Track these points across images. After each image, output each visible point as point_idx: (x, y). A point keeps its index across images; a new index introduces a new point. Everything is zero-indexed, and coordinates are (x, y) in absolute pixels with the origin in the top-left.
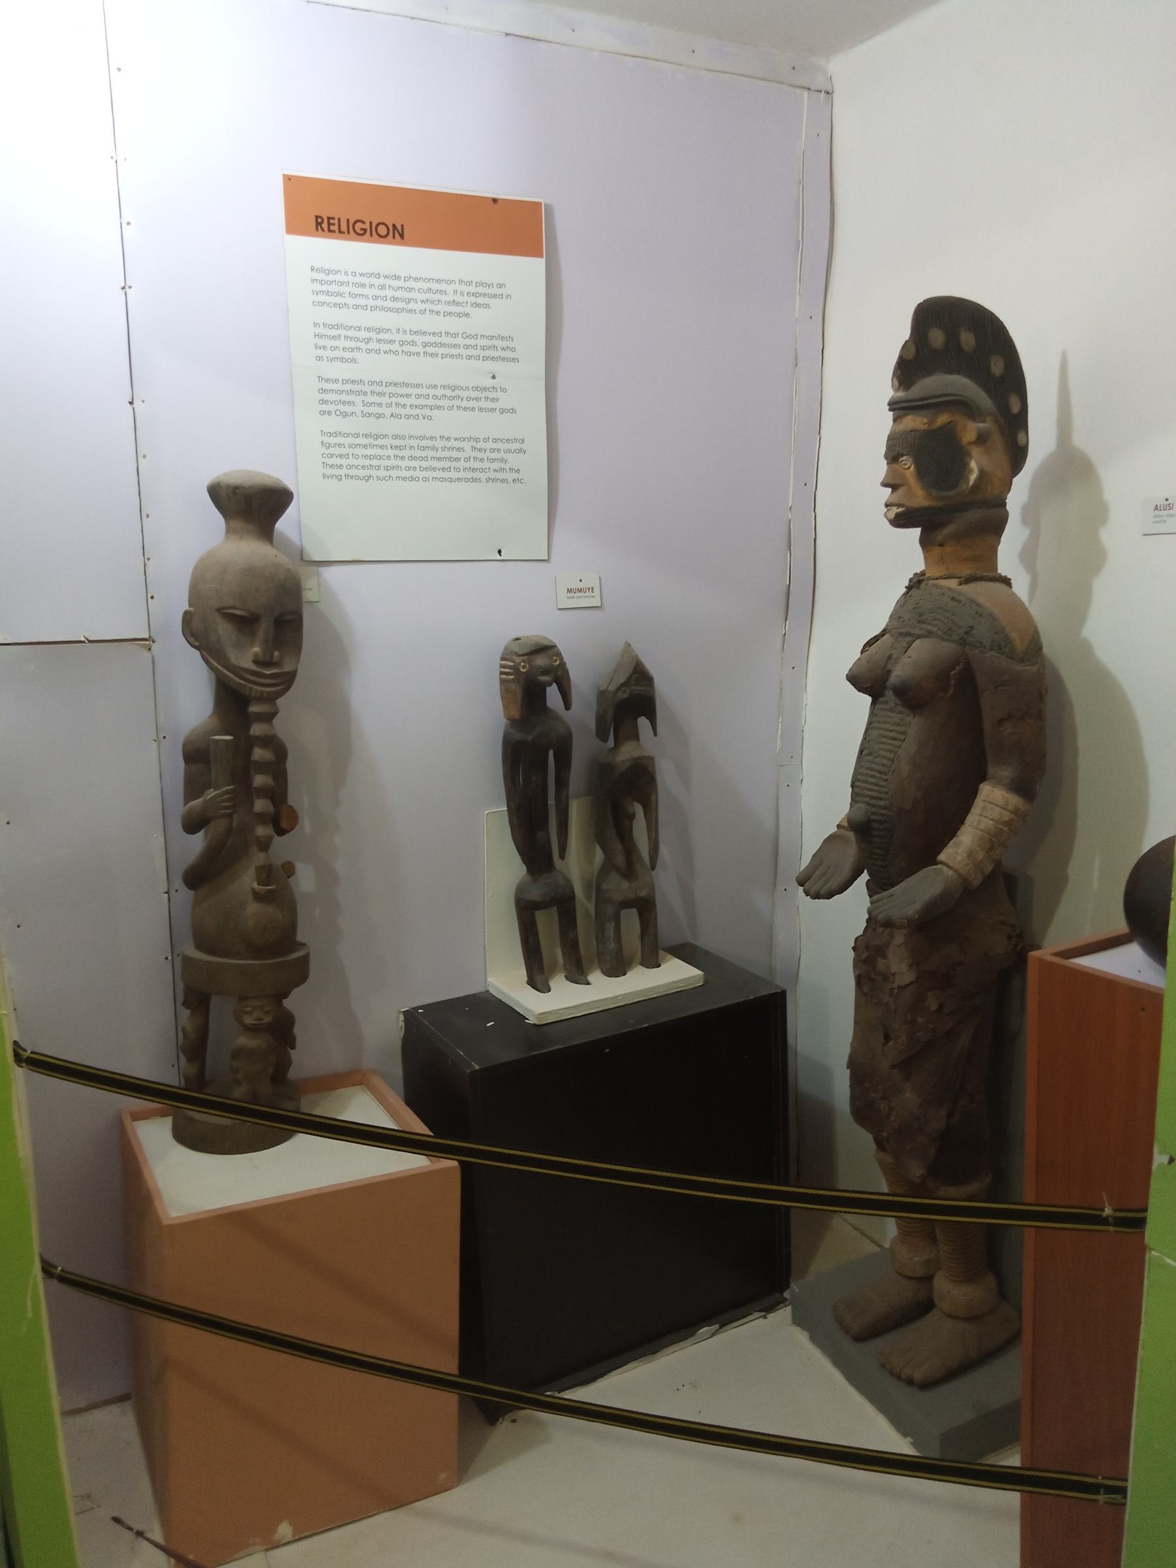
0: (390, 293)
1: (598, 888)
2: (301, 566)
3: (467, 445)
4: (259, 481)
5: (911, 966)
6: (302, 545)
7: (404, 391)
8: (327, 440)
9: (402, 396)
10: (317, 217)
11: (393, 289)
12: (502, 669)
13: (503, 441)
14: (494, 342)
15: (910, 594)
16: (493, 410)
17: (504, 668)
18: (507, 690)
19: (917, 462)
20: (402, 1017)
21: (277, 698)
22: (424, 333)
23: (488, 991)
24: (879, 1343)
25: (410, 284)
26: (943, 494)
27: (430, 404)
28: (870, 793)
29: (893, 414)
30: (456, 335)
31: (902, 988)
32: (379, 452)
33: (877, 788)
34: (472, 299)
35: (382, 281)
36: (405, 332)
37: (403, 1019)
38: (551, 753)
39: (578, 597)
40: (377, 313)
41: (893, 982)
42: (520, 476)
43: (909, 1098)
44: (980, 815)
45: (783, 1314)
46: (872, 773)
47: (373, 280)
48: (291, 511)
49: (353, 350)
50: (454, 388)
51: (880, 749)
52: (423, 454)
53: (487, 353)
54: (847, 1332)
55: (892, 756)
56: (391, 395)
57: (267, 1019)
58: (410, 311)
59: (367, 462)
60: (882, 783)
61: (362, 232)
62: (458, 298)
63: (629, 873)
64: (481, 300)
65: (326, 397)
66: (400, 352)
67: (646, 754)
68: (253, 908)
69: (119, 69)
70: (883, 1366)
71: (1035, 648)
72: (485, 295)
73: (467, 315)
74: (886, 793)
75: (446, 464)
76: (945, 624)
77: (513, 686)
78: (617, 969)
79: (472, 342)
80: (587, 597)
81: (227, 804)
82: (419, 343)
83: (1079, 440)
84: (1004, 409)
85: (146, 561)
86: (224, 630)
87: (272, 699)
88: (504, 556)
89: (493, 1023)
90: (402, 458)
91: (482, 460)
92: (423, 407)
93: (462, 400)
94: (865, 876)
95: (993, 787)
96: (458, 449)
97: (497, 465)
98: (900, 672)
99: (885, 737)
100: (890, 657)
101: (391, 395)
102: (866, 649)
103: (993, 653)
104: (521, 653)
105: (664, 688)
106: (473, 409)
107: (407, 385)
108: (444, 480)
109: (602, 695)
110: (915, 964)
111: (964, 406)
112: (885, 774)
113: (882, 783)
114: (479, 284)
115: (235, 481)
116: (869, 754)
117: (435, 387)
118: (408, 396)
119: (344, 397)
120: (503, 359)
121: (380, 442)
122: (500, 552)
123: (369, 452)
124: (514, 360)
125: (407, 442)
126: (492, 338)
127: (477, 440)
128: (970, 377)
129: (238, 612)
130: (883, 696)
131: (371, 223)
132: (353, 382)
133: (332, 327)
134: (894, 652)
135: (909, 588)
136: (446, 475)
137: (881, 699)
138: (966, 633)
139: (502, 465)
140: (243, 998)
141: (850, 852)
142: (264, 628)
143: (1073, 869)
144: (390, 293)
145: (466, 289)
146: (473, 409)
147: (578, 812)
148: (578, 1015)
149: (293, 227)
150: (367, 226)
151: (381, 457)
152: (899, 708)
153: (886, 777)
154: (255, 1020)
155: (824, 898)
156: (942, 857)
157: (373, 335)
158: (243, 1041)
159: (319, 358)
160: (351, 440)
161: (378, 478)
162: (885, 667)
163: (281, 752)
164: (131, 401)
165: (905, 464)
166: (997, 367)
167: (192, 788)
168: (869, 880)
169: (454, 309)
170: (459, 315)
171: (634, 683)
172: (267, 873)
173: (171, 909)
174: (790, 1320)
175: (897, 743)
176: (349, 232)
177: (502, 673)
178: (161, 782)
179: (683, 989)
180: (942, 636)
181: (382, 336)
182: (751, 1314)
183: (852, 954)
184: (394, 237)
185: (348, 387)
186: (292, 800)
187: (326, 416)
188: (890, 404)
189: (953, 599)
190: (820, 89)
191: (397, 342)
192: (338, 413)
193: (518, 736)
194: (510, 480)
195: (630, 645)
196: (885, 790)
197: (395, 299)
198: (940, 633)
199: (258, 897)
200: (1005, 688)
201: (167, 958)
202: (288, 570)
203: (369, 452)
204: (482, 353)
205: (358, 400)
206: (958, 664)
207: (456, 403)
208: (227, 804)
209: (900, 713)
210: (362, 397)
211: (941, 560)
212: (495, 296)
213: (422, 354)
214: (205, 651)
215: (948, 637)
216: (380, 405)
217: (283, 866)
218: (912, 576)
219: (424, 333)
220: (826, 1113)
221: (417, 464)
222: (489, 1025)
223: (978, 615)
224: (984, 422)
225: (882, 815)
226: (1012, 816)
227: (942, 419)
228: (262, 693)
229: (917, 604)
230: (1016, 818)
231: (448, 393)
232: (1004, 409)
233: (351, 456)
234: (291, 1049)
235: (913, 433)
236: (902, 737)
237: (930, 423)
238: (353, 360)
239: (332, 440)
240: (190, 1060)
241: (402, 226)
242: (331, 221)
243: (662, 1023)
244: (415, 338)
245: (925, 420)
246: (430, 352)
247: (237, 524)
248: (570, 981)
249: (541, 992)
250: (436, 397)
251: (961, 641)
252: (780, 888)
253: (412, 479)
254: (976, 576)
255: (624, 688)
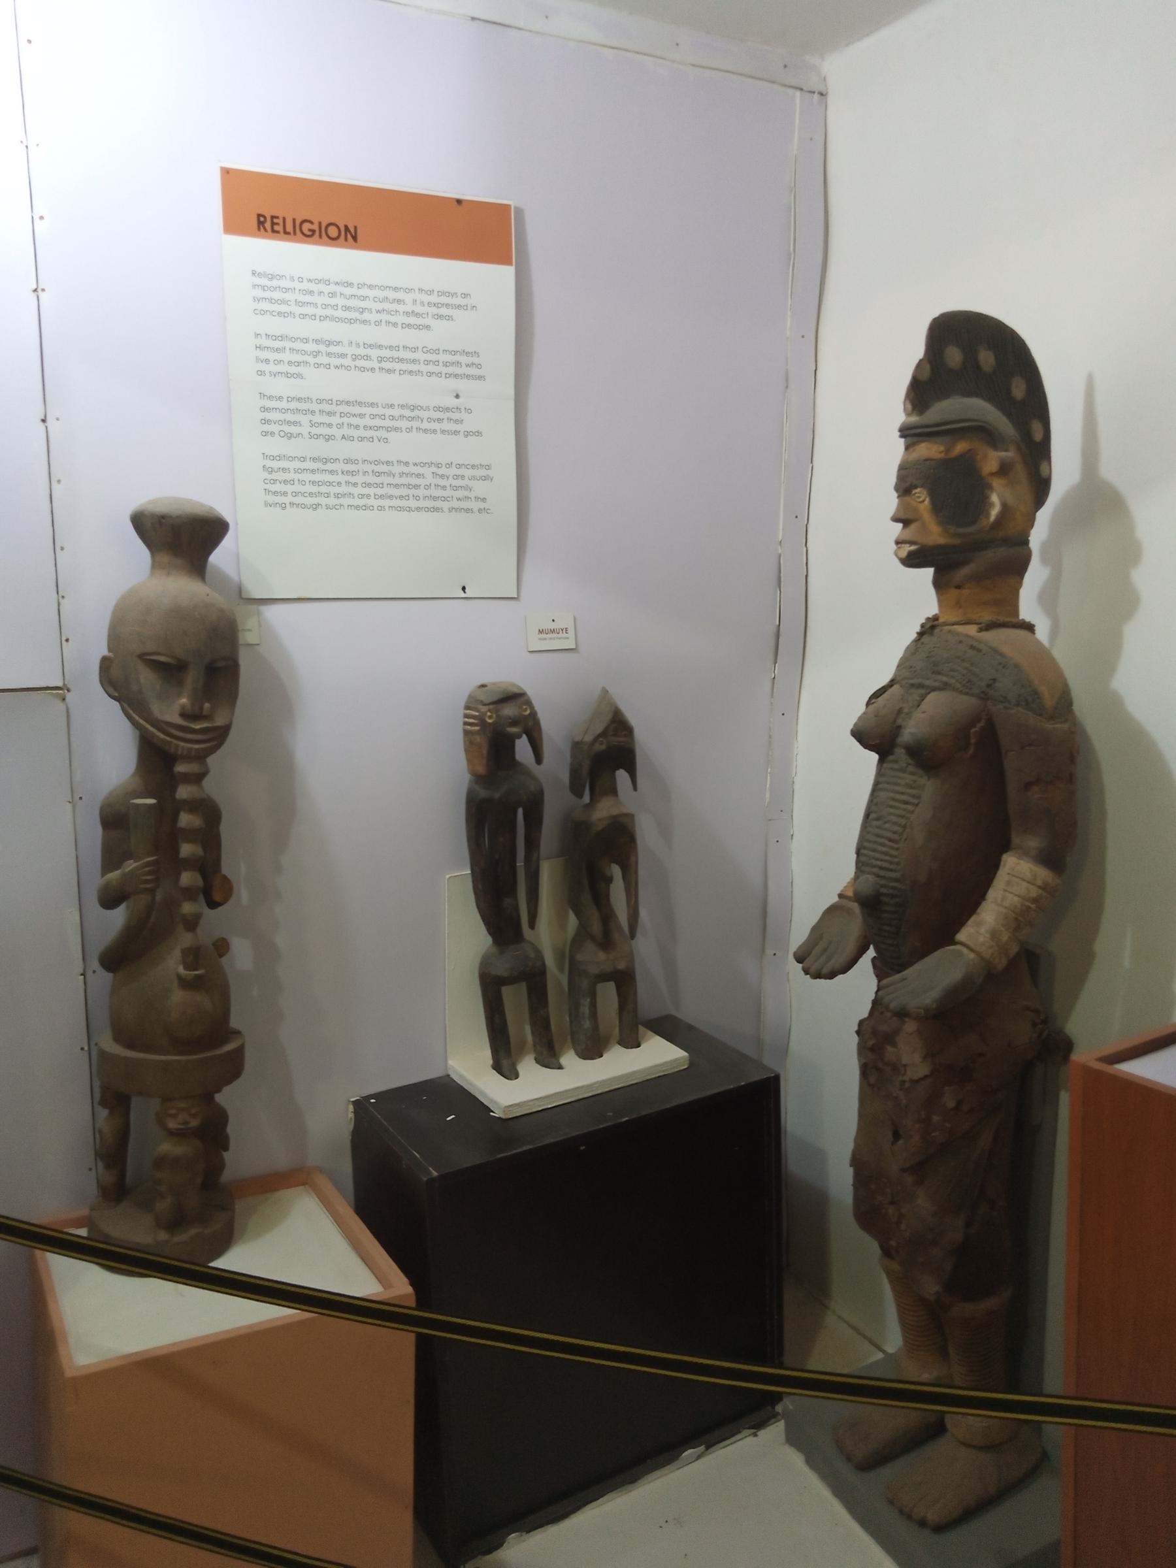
0: (341, 302)
1: (573, 962)
2: (238, 604)
3: (427, 471)
4: (189, 509)
5: (925, 1058)
6: (240, 581)
7: (356, 410)
8: (269, 463)
9: (354, 415)
10: (259, 216)
11: (345, 297)
12: (466, 720)
13: (468, 467)
14: (457, 358)
15: (922, 640)
16: (456, 433)
17: (468, 718)
18: (471, 743)
19: (932, 495)
20: (351, 1108)
21: (207, 756)
22: (380, 347)
23: (449, 1075)
24: (888, 1472)
25: (364, 292)
26: (961, 530)
27: (386, 425)
28: (879, 863)
29: (905, 441)
30: (415, 349)
31: (916, 1082)
32: (328, 478)
33: (887, 858)
34: (434, 310)
35: (332, 288)
36: (358, 345)
37: (353, 1110)
38: (520, 811)
39: (551, 639)
40: (327, 323)
41: (904, 1074)
42: (486, 505)
43: (923, 1204)
44: (1005, 890)
45: (776, 1431)
46: (882, 840)
47: (322, 287)
48: (227, 542)
49: (299, 364)
50: (413, 408)
51: (891, 814)
52: (378, 480)
53: (450, 370)
54: (849, 1459)
55: (904, 823)
56: (342, 415)
57: (194, 1123)
58: (364, 322)
59: (315, 489)
60: (894, 853)
61: (310, 233)
62: (418, 309)
63: (606, 943)
64: (444, 311)
65: (267, 416)
66: (353, 368)
67: (625, 811)
68: (178, 996)
69: (29, 41)
70: (891, 1502)
71: (1065, 704)
72: (447, 305)
73: (428, 327)
74: (898, 864)
75: (404, 491)
76: (964, 675)
77: (478, 739)
78: (592, 1050)
79: (433, 357)
80: (560, 638)
81: (149, 878)
82: (374, 357)
83: (1108, 471)
84: (1026, 435)
85: (60, 599)
86: (146, 678)
87: (201, 757)
88: (469, 593)
89: (453, 1116)
90: (355, 485)
91: (444, 488)
92: (378, 428)
93: (422, 421)
94: (871, 953)
95: (1019, 859)
96: (418, 475)
97: (460, 493)
98: (913, 729)
99: (894, 799)
100: (900, 711)
101: (342, 415)
102: (873, 701)
103: (1020, 709)
104: (488, 702)
105: (644, 738)
106: (434, 431)
107: (360, 404)
108: (401, 509)
109: (576, 746)
110: (929, 1055)
111: (986, 434)
112: (896, 842)
113: (894, 853)
114: (441, 293)
115: (161, 509)
116: (877, 819)
117: (392, 406)
118: (361, 416)
119: (290, 417)
120: (468, 377)
121: (329, 466)
122: (464, 589)
123: (318, 477)
124: (481, 378)
125: (361, 467)
126: (456, 353)
127: (439, 466)
128: (989, 400)
129: (162, 659)
130: (892, 754)
131: (320, 223)
132: (299, 400)
133: (276, 338)
134: (904, 705)
135: (921, 634)
136: (404, 503)
137: (891, 758)
138: (989, 686)
139: (466, 493)
140: (166, 1099)
141: (855, 925)
142: (192, 677)
143: (1101, 945)
144: (341, 302)
145: (426, 298)
146: (434, 431)
147: (549, 874)
148: (550, 1106)
149: (232, 226)
150: (316, 227)
151: (331, 484)
152: (911, 769)
153: (896, 846)
154: (179, 1124)
155: (825, 979)
156: (961, 936)
157: (322, 348)
158: (167, 1147)
159: (261, 373)
160: (297, 464)
161: (328, 507)
162: (895, 721)
163: (211, 814)
164: (43, 418)
165: (919, 497)
166: (1019, 389)
167: (112, 857)
168: (875, 957)
169: (412, 320)
170: (419, 327)
171: (612, 733)
172: (194, 956)
173: (88, 994)
174: (783, 1437)
175: (910, 807)
176: (295, 233)
177: (465, 724)
178: (76, 850)
179: (666, 1073)
180: (961, 689)
181: (332, 349)
182: (740, 1432)
183: (855, 1039)
184: (346, 240)
185: (293, 405)
186: (226, 870)
187: (269, 438)
188: (901, 430)
189: (972, 647)
190: (813, 90)
191: (349, 356)
192: (282, 434)
193: (483, 793)
194: (475, 510)
195: (608, 691)
196: (896, 860)
197: (347, 308)
198: (958, 685)
199: (184, 983)
200: (1032, 748)
201: (82, 1049)
202: (222, 610)
203: (318, 477)
204: (445, 370)
205: (305, 419)
206: (979, 720)
207: (415, 424)
208: (149, 878)
209: (912, 773)
210: (310, 417)
211: (958, 604)
212: (459, 307)
213: (377, 370)
214: (124, 702)
215: (967, 690)
216: (330, 425)
217: (214, 944)
218: (924, 621)
219: (380, 347)
220: (819, 1201)
221: (371, 491)
222: (448, 1119)
223: (1001, 666)
224: (1006, 450)
225: (893, 888)
226: (1040, 891)
227: (961, 447)
228: (190, 750)
229: (931, 652)
230: (1045, 894)
231: (407, 413)
232: (1026, 435)
233: (296, 482)
234: (225, 1151)
235: (928, 462)
236: (916, 801)
237: (947, 451)
238: (299, 376)
239: (275, 464)
240: (108, 1166)
241: (355, 227)
242: (275, 221)
243: (646, 1116)
244: (369, 351)
245: (942, 448)
246: (387, 368)
247: (165, 558)
248: (541, 1065)
249: (508, 1079)
250: (393, 418)
251: (982, 695)
252: (769, 952)
253: (366, 507)
254: (998, 622)
255: (601, 739)
